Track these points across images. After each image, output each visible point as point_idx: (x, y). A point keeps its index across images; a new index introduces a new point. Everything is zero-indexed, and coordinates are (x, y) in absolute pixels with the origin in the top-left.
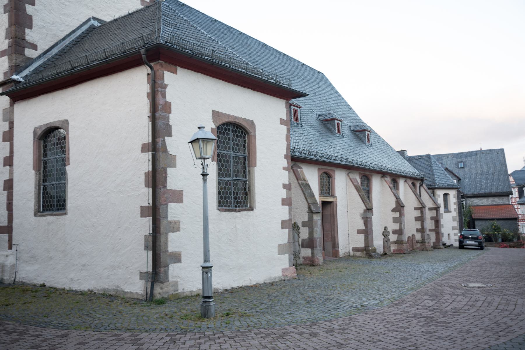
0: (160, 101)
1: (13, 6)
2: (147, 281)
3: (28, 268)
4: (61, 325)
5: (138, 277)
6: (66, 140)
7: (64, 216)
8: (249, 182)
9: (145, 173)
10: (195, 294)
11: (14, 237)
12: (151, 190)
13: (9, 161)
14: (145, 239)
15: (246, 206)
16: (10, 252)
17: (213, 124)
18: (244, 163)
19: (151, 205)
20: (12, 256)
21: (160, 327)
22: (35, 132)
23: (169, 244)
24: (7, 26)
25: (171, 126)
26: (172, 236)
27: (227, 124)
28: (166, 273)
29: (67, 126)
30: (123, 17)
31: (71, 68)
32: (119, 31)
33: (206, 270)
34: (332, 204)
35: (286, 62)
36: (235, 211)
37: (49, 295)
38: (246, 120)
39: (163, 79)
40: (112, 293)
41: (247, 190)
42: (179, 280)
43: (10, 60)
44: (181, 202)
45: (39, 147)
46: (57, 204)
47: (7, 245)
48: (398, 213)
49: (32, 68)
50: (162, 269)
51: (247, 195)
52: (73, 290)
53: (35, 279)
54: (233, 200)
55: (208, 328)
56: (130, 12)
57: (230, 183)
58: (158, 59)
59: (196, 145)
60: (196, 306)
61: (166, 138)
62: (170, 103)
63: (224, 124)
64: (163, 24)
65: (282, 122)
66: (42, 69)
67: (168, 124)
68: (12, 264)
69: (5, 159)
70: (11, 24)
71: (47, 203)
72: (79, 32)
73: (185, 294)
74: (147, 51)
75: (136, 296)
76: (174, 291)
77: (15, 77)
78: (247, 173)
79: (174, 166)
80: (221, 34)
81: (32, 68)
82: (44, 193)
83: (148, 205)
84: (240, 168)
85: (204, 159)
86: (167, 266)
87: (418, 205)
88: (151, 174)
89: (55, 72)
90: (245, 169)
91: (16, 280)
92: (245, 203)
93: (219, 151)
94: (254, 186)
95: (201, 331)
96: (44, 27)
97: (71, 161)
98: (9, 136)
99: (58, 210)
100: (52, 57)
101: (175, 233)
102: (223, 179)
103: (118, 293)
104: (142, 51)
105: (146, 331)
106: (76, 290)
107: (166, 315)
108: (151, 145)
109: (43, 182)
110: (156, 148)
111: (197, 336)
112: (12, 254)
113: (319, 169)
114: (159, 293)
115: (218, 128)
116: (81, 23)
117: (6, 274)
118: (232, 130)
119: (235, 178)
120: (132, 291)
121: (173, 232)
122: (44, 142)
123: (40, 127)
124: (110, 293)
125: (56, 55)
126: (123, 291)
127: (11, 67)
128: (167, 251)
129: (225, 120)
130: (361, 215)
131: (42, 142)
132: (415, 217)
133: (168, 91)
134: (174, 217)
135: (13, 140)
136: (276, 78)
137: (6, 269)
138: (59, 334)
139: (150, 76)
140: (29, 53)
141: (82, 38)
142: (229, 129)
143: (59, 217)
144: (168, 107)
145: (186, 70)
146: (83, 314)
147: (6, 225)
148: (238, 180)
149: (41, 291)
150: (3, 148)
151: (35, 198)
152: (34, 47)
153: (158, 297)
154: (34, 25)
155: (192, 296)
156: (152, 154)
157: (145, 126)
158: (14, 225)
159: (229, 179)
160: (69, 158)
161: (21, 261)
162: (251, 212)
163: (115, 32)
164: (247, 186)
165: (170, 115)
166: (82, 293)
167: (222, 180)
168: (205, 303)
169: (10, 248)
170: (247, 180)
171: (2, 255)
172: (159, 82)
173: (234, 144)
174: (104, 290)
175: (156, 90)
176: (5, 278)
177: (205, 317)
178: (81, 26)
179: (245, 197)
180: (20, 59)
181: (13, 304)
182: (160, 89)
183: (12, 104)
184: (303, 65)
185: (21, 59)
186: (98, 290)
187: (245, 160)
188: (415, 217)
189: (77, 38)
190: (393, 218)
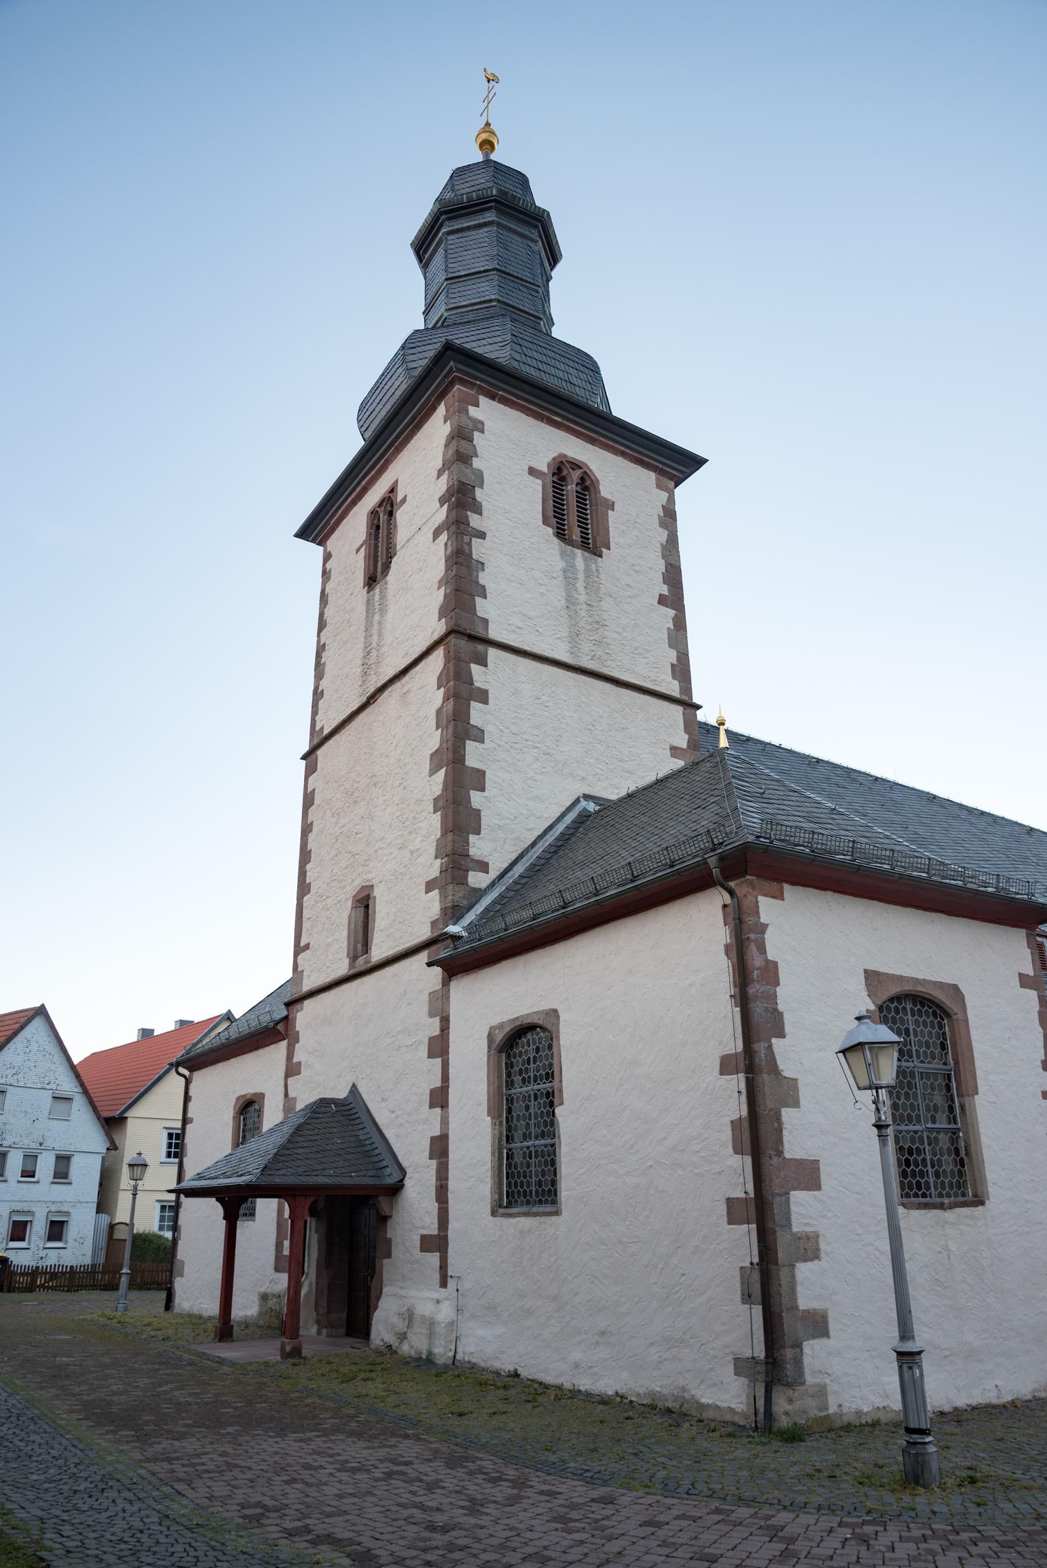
0: (756, 961)
1: (450, 797)
2: (754, 1381)
3: (481, 1332)
4: (588, 1474)
5: (731, 1368)
6: (555, 1049)
7: (554, 1218)
8: (966, 1133)
9: (732, 1122)
10: (870, 1421)
11: (450, 1261)
12: (748, 1160)
13: (440, 1098)
14: (742, 1277)
15: (964, 1195)
16: (443, 1293)
17: (868, 1000)
18: (948, 1088)
19: (752, 1195)
20: (447, 1303)
21: (816, 1500)
22: (490, 1037)
23: (800, 1290)
24: (439, 836)
26: (804, 1270)
27: (898, 998)
28: (798, 1362)
29: (555, 1021)
30: (645, 789)
31: (562, 904)
32: (645, 819)
33: (908, 1359)
35: (990, 829)
36: (942, 1207)
37: (535, 1400)
38: (940, 985)
39: (757, 913)
40: (670, 1404)
41: (963, 1153)
42: (827, 1381)
43: (443, 896)
44: (818, 1187)
45: (499, 1067)
46: (537, 1191)
47: (437, 1276)
49: (479, 908)
50: (789, 1353)
51: (963, 1165)
52: (580, 1391)
53: (497, 1358)
54: (932, 1180)
55: (934, 1513)
56: (661, 775)
57: (921, 1138)
58: (745, 873)
59: (855, 1057)
60: (892, 1454)
61: (774, 1040)
62: (776, 964)
63: (891, 1000)
64: (739, 797)
65: (1025, 981)
66: (498, 907)
67: (776, 1010)
68: (449, 1320)
69: (433, 1092)
70: (445, 831)
71: (516, 1187)
72: (560, 828)
73: (845, 1419)
74: (722, 858)
75: (728, 1417)
76: (820, 1410)
77: (453, 929)
78: (958, 1110)
79: (796, 1104)
80: (834, 789)
81: (479, 908)
82: (509, 1166)
83: (743, 1195)
84: (939, 1099)
85: (877, 1089)
86: (798, 1345)
88: (746, 1125)
89: (527, 914)
90: (953, 1101)
91: (458, 1357)
92: (961, 1186)
93: (904, 1064)
94: (978, 1141)
95: (918, 1520)
96: (500, 827)
97: (565, 1096)
98: (439, 1047)
99: (540, 1202)
100: (515, 883)
101: (809, 1264)
102: (903, 1127)
103: (686, 1406)
104: (712, 861)
105: (785, 1507)
106: (586, 1391)
107: (819, 1471)
108: (741, 1058)
109: (508, 1141)
110: (753, 1062)
111: (917, 1533)
112: (448, 1299)
114: (787, 1414)
115: (880, 1008)
116: (564, 809)
117: (437, 1342)
118: (911, 1009)
119: (930, 1125)
120: (718, 1403)
121: (805, 1261)
122: (508, 1057)
123: (501, 1026)
124: (667, 1405)
125: (521, 876)
126: (697, 1402)
127: (444, 910)
128: (796, 1308)
129: (895, 990)
131: (504, 1056)
133: (771, 938)
134: (806, 1225)
135: (447, 1053)
136: (998, 882)
137: (438, 1330)
138: (595, 1494)
139: (730, 910)
140: (477, 879)
141: (566, 838)
142: (904, 1008)
143: (543, 1219)
144: (771, 972)
145: (801, 889)
146: (625, 1451)
147: (436, 1232)
148: (938, 1131)
149: (514, 1387)
150: (429, 1071)
151: (493, 1177)
152: (484, 867)
153: (784, 1422)
154: (483, 827)
155: (861, 1425)
156: (747, 1079)
157: (725, 1017)
158: (451, 1234)
159: (918, 1128)
160: (561, 1091)
161: (467, 1315)
162: (980, 1208)
163: (636, 822)
164: (962, 1144)
165: (778, 989)
166: (604, 1401)
167: (901, 1132)
168: (913, 1449)
169: (444, 1284)
170: (959, 1129)
171: (428, 1299)
172: (750, 920)
173: (920, 1043)
174: (653, 1395)
176: (436, 1351)
177: (917, 1483)
178: (563, 815)
179: (960, 1171)
180: (461, 892)
181: (471, 1413)
182: (752, 936)
183: (446, 983)
184: (1031, 830)
185: (462, 894)
186: (638, 1395)
187: (950, 1080)
189: (557, 839)
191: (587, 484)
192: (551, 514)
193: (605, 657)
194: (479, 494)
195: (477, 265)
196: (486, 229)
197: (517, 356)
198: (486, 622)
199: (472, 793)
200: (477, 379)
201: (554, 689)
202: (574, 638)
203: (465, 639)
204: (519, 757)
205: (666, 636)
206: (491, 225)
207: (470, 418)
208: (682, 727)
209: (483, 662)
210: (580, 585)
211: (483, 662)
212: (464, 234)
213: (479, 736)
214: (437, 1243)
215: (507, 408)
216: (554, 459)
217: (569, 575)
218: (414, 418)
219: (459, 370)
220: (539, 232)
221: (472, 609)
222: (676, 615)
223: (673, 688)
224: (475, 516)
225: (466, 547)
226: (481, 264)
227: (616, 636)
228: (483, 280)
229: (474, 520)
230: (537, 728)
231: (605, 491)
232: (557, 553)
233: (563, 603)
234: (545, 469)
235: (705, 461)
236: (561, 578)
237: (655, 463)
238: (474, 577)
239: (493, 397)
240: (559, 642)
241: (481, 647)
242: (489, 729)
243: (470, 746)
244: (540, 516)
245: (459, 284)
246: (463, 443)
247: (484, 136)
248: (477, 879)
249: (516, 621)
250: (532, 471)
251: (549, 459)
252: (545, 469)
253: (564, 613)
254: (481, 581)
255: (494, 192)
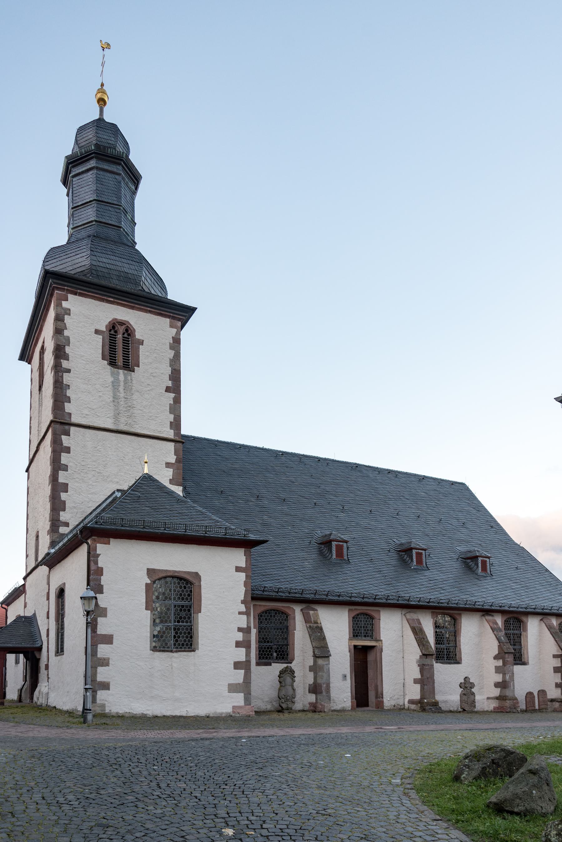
0: (93, 567)
23: (98, 675)
25: (102, 586)
34: (375, 649)
36: (171, 651)
38: (189, 573)
44: (112, 643)
48: (501, 661)
56: (130, 485)
81: (66, 539)
87: (558, 651)
96: (75, 507)
101: (104, 668)
113: (349, 610)
128: (96, 680)
130: (417, 661)
132: (554, 668)
133: (100, 559)
140: (63, 530)
152: (67, 524)
162: (192, 653)
172: (92, 553)
175: (92, 557)
180: (56, 536)
188: (554, 668)
190: (496, 667)
191: (129, 332)
192: (107, 353)
193: (133, 423)
194: (68, 350)
195: (87, 197)
196: (91, 172)
197: (94, 263)
198: (70, 414)
199: (61, 494)
200: (65, 286)
201: (104, 442)
202: (116, 417)
203: (61, 424)
204: (85, 476)
205: (168, 408)
206: (102, 162)
207: (63, 308)
208: (173, 453)
209: (68, 434)
210: (121, 389)
211: (68, 434)
212: (81, 177)
213: (65, 468)
214: (47, 667)
215: (83, 298)
216: (110, 322)
217: (115, 385)
218: (45, 306)
219: (55, 283)
220: (123, 166)
221: (63, 409)
222: (175, 396)
223: (170, 434)
224: (65, 361)
225: (60, 378)
226: (89, 196)
227: (139, 412)
228: (89, 207)
229: (65, 364)
230: (94, 462)
231: (138, 335)
232: (109, 373)
233: (111, 399)
234: (104, 329)
235: (193, 310)
236: (111, 387)
237: (168, 314)
238: (64, 394)
239: (75, 294)
240: (108, 419)
241: (67, 427)
242: (70, 465)
243: (61, 473)
244: (101, 356)
245: (78, 211)
246: (59, 323)
247: (99, 95)
248: (63, 530)
249: (86, 412)
250: (97, 332)
251: (107, 323)
252: (104, 329)
253: (111, 404)
254: (68, 395)
255: (93, 148)
